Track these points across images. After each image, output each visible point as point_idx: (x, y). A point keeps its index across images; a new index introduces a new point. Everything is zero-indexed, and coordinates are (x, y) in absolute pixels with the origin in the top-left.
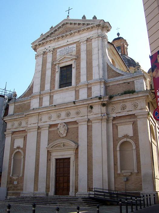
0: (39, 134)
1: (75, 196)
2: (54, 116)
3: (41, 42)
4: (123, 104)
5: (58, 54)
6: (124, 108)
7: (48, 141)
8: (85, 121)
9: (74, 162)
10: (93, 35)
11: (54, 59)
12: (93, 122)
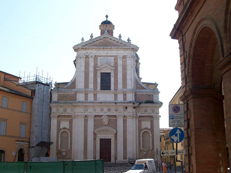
0: (86, 121)
1: (115, 162)
2: (98, 109)
5: (99, 61)
6: (146, 111)
11: (95, 66)
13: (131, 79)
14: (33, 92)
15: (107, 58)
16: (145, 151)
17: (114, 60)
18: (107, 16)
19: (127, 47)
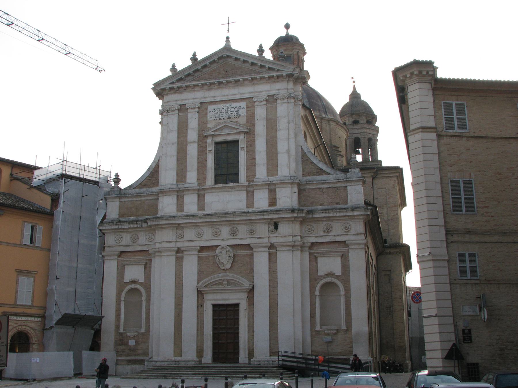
1: (249, 364)
3: (175, 86)
4: (327, 223)
5: (210, 115)
6: (328, 230)
7: (198, 273)
8: (266, 247)
9: (247, 311)
10: (281, 91)
12: (278, 249)
13: (288, 151)
14: (55, 199)
15: (228, 105)
16: (328, 334)
17: (247, 108)
18: (287, 26)
19: (275, 74)
